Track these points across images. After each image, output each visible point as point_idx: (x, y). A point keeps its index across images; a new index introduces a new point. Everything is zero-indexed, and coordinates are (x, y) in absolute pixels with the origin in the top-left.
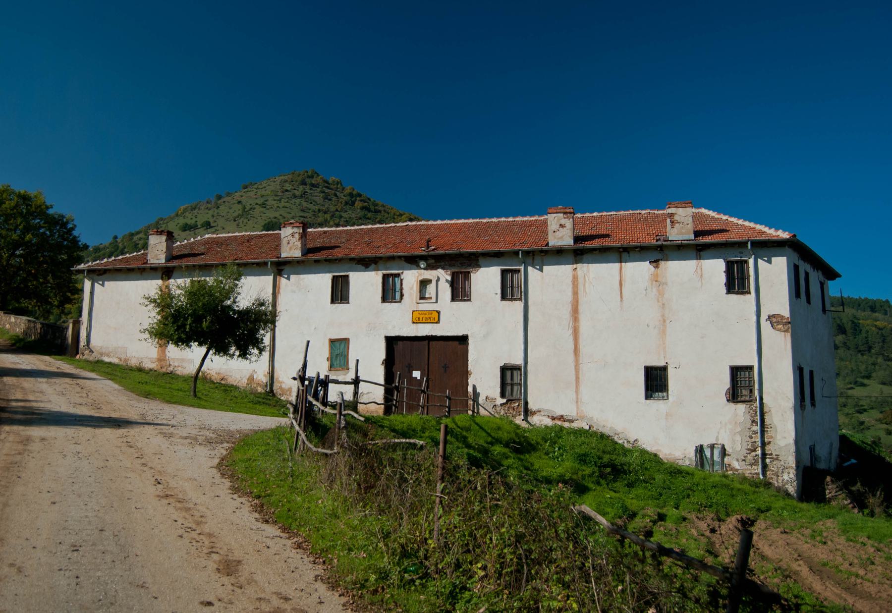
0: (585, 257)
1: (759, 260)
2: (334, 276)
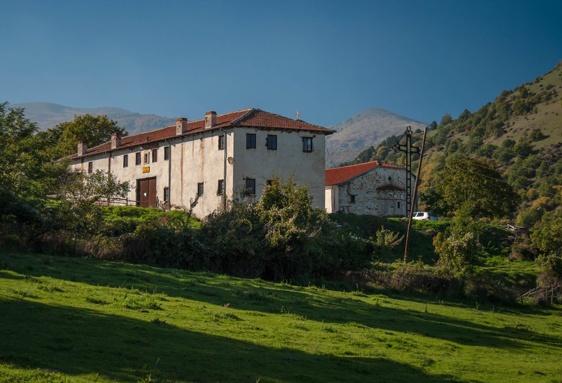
0: (185, 139)
1: (172, 146)
2: (247, 134)
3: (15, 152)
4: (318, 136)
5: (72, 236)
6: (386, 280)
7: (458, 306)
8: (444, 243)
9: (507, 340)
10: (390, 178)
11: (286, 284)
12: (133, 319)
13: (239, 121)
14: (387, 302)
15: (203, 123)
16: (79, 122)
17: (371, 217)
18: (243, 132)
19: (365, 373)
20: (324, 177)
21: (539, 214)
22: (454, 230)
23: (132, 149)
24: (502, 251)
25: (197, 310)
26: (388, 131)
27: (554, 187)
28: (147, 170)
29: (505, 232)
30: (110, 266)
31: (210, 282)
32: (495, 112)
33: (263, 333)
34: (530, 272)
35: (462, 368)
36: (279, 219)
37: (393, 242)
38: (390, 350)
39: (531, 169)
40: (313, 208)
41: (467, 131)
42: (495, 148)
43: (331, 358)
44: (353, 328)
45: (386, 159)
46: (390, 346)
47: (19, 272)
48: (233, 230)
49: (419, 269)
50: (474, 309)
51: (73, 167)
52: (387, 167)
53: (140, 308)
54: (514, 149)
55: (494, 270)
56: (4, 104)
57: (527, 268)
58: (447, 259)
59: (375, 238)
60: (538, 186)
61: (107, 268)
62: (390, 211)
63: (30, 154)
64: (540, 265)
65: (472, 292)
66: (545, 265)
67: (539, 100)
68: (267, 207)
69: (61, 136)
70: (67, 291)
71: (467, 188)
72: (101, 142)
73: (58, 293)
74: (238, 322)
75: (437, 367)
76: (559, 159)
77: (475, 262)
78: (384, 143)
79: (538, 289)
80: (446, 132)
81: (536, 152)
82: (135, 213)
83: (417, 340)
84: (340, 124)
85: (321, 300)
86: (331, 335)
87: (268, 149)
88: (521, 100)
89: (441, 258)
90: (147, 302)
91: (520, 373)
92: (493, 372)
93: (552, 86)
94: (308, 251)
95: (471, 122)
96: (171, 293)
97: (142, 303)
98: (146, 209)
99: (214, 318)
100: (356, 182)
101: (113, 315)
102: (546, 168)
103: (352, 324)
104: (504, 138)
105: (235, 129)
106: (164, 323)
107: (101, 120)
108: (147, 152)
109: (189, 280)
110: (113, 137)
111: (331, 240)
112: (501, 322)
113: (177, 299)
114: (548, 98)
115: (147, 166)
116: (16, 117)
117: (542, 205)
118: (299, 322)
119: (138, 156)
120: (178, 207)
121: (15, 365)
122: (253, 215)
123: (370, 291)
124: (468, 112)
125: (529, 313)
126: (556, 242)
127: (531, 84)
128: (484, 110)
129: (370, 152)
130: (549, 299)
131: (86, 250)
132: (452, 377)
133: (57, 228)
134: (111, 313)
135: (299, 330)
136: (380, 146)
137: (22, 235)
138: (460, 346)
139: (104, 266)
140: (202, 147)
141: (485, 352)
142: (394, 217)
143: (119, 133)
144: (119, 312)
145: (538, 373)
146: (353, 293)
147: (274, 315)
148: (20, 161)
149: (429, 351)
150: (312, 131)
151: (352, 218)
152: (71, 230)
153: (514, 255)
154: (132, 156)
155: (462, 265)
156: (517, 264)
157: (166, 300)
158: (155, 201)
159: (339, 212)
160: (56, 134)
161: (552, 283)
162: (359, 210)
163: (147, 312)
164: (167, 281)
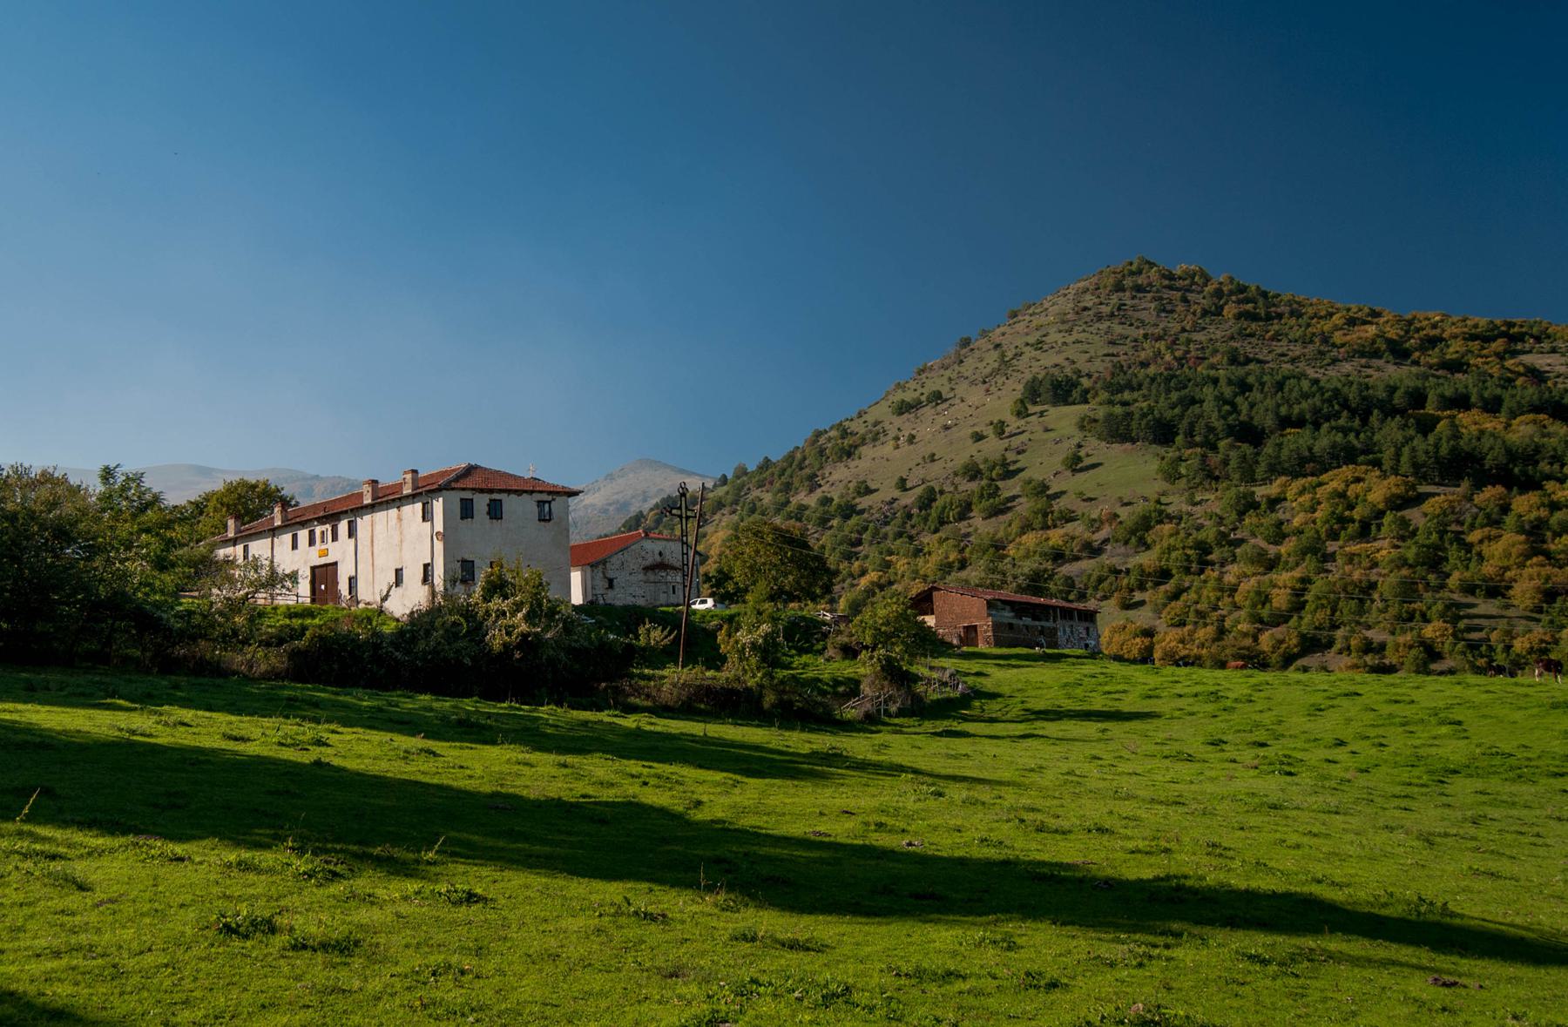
0: (376, 508)
2: (462, 500)
3: (131, 534)
4: (558, 499)
5: (215, 649)
6: (654, 694)
7: (752, 725)
8: (732, 640)
9: (812, 769)
10: (660, 554)
11: (513, 704)
12: (286, 761)
13: (450, 482)
14: (652, 724)
15: (400, 486)
16: (231, 489)
17: (635, 606)
18: (456, 497)
19: (603, 822)
20: (569, 553)
21: (870, 592)
22: (745, 621)
23: (303, 524)
24: (815, 648)
25: (380, 744)
26: (662, 490)
27: (888, 558)
28: (325, 553)
29: (818, 622)
30: (267, 688)
31: (405, 706)
32: (804, 459)
33: (468, 772)
34: (852, 675)
35: (741, 809)
36: (504, 613)
37: (662, 640)
38: (646, 789)
39: (856, 536)
40: (551, 597)
41: (768, 486)
42: (805, 508)
43: (558, 804)
44: (597, 760)
45: (661, 528)
46: (645, 784)
47: (133, 701)
48: (441, 632)
49: (700, 676)
50: (773, 729)
51: (221, 553)
52: (656, 539)
53: (298, 745)
54: (832, 509)
55: (802, 674)
56: (116, 467)
57: (846, 669)
58: (736, 660)
59: (637, 637)
60: (866, 557)
61: (262, 691)
62: (663, 599)
63: (152, 536)
64: (864, 664)
65: (773, 706)
66: (872, 665)
67: (863, 442)
68: (486, 599)
69: (205, 510)
70: (198, 725)
71: (764, 564)
72: (261, 516)
73: (182, 729)
74: (436, 759)
75: (706, 810)
76: (892, 520)
77: (776, 664)
78: (657, 506)
79: (863, 698)
80: (740, 488)
81: (862, 512)
82: (307, 613)
83: (685, 773)
84: (597, 481)
85: (560, 724)
86: (565, 771)
87: (491, 518)
88: (840, 441)
89: (729, 660)
90: (310, 735)
91: (821, 814)
92: (784, 814)
93: (880, 422)
94: (544, 657)
95: (773, 474)
96: (347, 723)
97: (301, 738)
98: (325, 607)
99: (402, 754)
100: (614, 560)
101: (258, 756)
102: (876, 533)
103: (598, 755)
104: (818, 493)
105: (444, 492)
106: (328, 764)
107: (261, 486)
108: (324, 528)
109: (375, 703)
110: (277, 509)
111: (576, 641)
112: (807, 745)
113: (355, 730)
114: (875, 439)
115: (324, 547)
116: (134, 485)
117: (873, 583)
118: (521, 756)
119: (312, 533)
120: (368, 604)
121: (99, 832)
122: (468, 610)
123: (634, 709)
124: (769, 460)
125: (852, 731)
126: (885, 633)
127: (852, 420)
128: (790, 457)
129: (638, 519)
130: (878, 711)
131: (235, 667)
132: (724, 822)
133: (194, 638)
134: (255, 753)
135: (521, 767)
136: (652, 510)
137: (144, 650)
138: (746, 780)
139: (258, 689)
140: (400, 519)
141: (779, 787)
142: (668, 606)
143: (285, 503)
144: (265, 752)
145: (847, 812)
146: (606, 712)
147: (488, 747)
148: (137, 547)
149: (700, 789)
150: (550, 493)
151: (609, 610)
152: (214, 640)
153: (831, 652)
154: (303, 534)
155: (758, 669)
156: (836, 665)
157: (338, 733)
158: (336, 596)
159: (591, 602)
160: (199, 507)
161: (882, 689)
162: (619, 598)
163: (307, 750)
164: (346, 706)
